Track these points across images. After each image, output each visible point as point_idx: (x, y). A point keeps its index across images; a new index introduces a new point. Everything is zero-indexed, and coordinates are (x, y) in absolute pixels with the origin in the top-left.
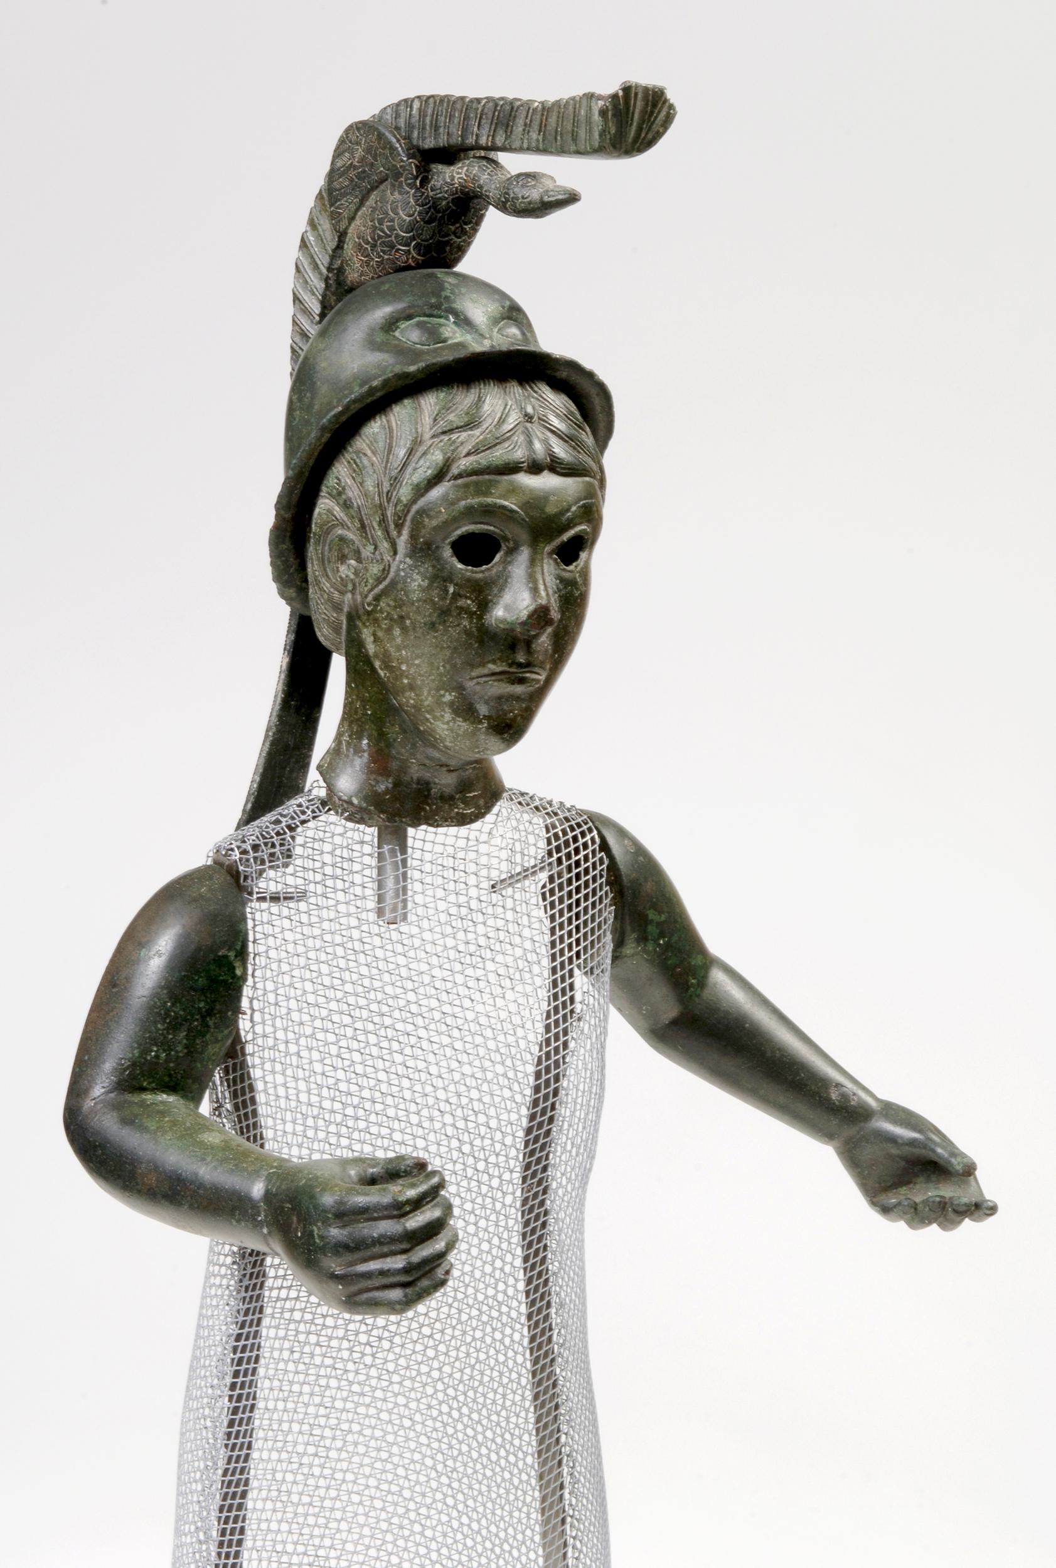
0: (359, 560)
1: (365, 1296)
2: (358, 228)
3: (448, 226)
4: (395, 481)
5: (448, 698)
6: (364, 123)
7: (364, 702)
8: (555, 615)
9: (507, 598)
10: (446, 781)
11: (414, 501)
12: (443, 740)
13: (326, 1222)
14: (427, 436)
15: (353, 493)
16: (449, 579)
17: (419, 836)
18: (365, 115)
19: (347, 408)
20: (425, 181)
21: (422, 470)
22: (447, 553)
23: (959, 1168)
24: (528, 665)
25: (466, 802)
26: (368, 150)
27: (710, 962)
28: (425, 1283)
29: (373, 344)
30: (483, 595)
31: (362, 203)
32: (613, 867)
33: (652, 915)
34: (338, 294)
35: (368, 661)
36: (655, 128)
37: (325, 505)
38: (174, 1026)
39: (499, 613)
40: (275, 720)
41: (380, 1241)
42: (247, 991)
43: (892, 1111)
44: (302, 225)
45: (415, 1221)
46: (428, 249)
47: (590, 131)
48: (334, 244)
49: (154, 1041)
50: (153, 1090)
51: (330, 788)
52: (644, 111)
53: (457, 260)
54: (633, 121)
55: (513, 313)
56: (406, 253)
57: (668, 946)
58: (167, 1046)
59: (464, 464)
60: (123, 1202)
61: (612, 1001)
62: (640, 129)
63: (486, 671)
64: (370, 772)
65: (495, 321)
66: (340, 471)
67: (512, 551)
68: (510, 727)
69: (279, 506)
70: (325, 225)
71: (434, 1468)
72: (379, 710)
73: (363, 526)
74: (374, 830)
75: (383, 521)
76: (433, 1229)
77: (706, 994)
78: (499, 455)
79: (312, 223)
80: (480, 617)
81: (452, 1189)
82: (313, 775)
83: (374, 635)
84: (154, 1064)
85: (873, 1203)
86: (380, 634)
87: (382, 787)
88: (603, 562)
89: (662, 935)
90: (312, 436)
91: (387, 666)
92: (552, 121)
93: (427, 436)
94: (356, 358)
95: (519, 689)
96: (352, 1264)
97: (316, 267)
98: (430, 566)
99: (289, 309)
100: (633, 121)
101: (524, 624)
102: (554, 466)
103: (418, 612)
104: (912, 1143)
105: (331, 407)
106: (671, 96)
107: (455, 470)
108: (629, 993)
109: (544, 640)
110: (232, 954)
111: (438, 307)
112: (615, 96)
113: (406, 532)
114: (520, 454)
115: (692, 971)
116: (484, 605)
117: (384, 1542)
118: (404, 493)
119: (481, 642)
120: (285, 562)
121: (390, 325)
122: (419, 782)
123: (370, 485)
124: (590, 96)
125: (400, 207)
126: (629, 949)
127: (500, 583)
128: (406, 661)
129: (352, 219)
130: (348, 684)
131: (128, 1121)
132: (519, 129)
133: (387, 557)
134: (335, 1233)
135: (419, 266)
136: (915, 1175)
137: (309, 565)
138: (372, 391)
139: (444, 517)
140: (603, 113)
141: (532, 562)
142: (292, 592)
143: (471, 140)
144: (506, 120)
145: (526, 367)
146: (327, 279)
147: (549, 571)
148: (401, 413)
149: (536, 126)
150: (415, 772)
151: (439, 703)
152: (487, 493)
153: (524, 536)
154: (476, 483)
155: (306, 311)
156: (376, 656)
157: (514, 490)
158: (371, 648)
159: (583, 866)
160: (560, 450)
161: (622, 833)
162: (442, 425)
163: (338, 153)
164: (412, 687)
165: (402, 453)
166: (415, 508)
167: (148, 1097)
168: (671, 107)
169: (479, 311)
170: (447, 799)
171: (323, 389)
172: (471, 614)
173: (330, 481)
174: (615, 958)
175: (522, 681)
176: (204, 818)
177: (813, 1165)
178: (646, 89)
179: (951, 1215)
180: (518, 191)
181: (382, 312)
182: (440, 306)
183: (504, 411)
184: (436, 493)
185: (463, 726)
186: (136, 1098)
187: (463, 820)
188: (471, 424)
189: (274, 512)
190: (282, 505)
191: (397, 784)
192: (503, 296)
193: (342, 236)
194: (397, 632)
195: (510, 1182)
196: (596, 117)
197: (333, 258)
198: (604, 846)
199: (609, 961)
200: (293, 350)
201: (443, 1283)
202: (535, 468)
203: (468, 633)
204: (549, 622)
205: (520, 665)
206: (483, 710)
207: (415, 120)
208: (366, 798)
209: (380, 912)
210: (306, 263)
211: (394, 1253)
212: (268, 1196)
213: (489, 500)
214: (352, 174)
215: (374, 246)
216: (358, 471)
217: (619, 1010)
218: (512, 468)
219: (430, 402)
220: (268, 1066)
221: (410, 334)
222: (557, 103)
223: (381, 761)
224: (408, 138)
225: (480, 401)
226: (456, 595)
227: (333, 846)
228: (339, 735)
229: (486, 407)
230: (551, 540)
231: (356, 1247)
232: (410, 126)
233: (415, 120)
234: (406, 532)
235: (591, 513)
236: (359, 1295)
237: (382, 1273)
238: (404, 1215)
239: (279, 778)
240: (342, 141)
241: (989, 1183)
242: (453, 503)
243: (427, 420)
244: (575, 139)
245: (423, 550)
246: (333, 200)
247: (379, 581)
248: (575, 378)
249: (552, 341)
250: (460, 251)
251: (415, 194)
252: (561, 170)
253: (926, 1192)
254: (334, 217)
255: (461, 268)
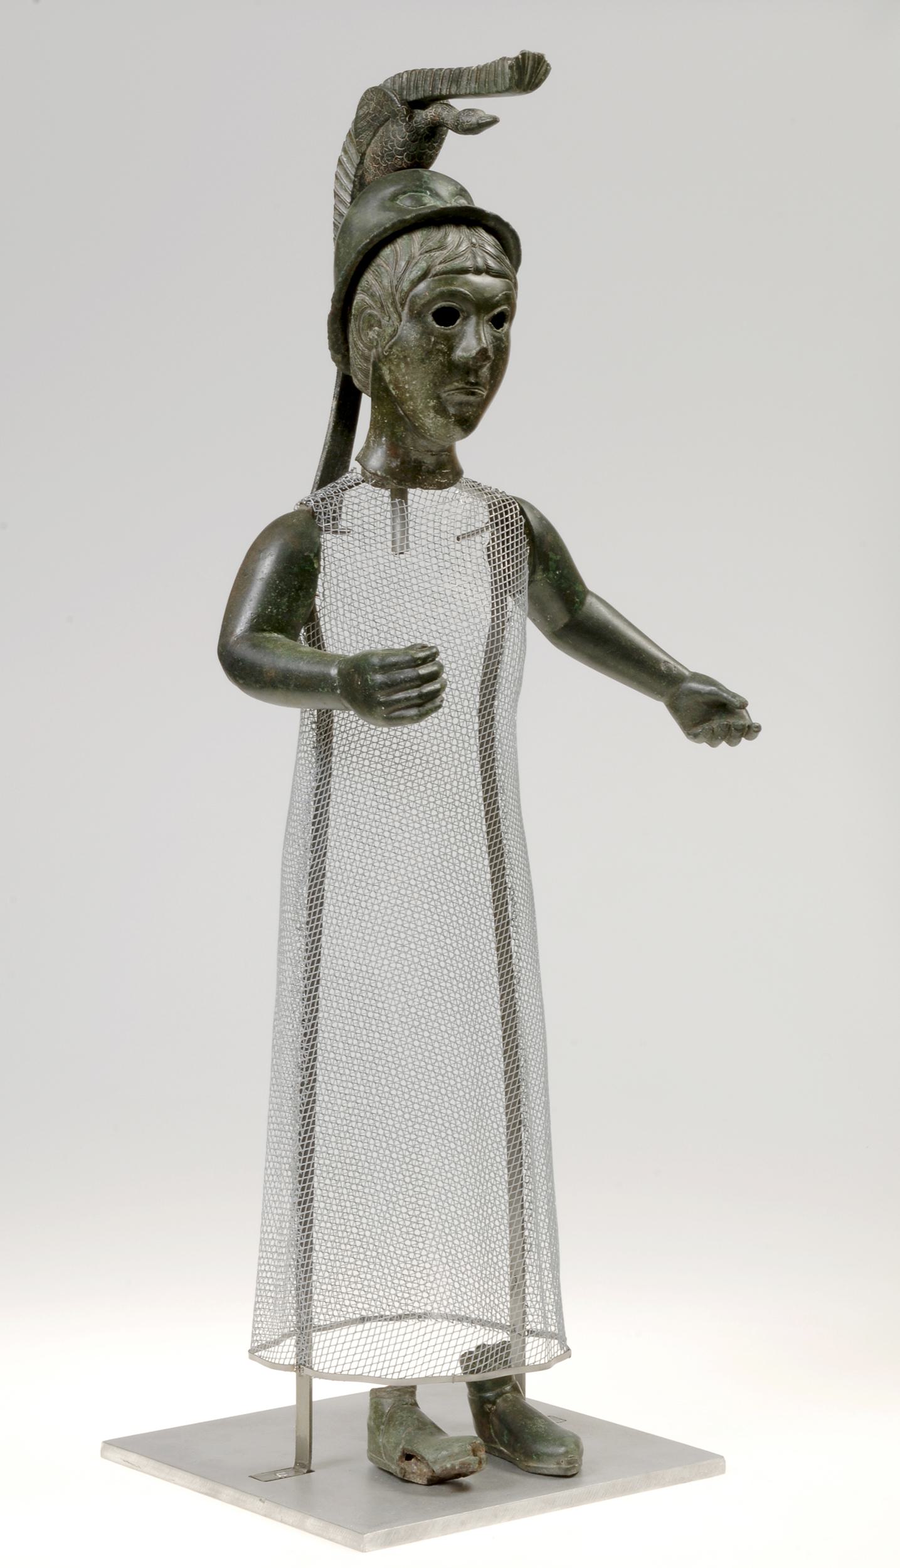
0: (380, 326)
1: (397, 713)
2: (374, 148)
3: (423, 146)
4: (400, 280)
5: (432, 403)
6: (375, 88)
7: (382, 415)
8: (490, 354)
9: (464, 344)
10: (429, 461)
11: (411, 290)
12: (429, 430)
13: (375, 672)
14: (417, 254)
15: (377, 289)
16: (431, 333)
17: (415, 495)
18: (377, 82)
19: (372, 240)
20: (411, 118)
21: (415, 273)
22: (430, 319)
23: (737, 704)
24: (477, 384)
25: (443, 476)
26: (378, 104)
27: (586, 592)
28: (429, 706)
29: (384, 208)
30: (451, 343)
31: (374, 135)
32: (528, 524)
33: (551, 555)
34: (360, 187)
35: (386, 390)
36: (539, 77)
37: (360, 297)
38: (281, 595)
39: (459, 354)
40: (329, 438)
41: (404, 681)
42: (321, 576)
43: (696, 677)
44: (339, 152)
45: (423, 671)
46: (413, 157)
47: (504, 79)
48: (358, 161)
49: (270, 603)
50: (270, 631)
51: (364, 467)
52: (533, 67)
53: (430, 164)
54: (527, 73)
55: (462, 192)
56: (402, 159)
57: (561, 576)
58: (277, 606)
59: (438, 268)
60: (256, 697)
61: (529, 615)
62: (531, 77)
63: (453, 387)
64: (388, 456)
65: (454, 195)
66: (369, 277)
67: (466, 318)
68: (467, 424)
69: (333, 301)
70: (352, 151)
71: (429, 910)
72: (394, 421)
73: (382, 306)
74: (388, 493)
75: (394, 303)
76: (433, 677)
77: (584, 609)
78: (457, 263)
79: (345, 150)
80: (449, 355)
81: (442, 655)
82: (353, 464)
83: (390, 369)
84: (270, 616)
85: (688, 734)
86: (393, 368)
87: (394, 465)
88: (518, 331)
89: (557, 568)
90: (352, 257)
91: (397, 388)
92: (483, 76)
93: (417, 254)
94: (374, 216)
95: (472, 398)
96: (389, 695)
97: (347, 175)
98: (420, 333)
99: (332, 201)
100: (527, 73)
101: (474, 358)
102: (488, 271)
103: (414, 353)
104: (710, 693)
105: (360, 241)
106: (548, 59)
107: (433, 272)
108: (538, 610)
109: (485, 371)
110: (312, 555)
111: (421, 186)
112: (517, 58)
113: (406, 308)
114: (469, 264)
115: (575, 593)
116: (451, 348)
117: (409, 902)
118: (405, 285)
119: (450, 370)
120: (336, 336)
121: (394, 197)
122: (416, 461)
123: (386, 282)
124: (504, 59)
125: (397, 133)
126: (539, 576)
127: (461, 336)
128: (408, 383)
129: (368, 145)
130: (373, 407)
131: (255, 646)
132: (464, 83)
133: (396, 323)
134: (379, 678)
135: (408, 168)
136: (713, 714)
137: (350, 336)
138: (386, 230)
139: (428, 298)
140: (511, 67)
141: (478, 324)
142: (339, 357)
143: (437, 93)
144: (458, 81)
145: (469, 217)
146: (354, 182)
147: (487, 334)
148: (401, 243)
149: (474, 78)
150: (414, 455)
151: (427, 407)
152: (451, 284)
153: (472, 309)
154: (446, 279)
155: (342, 202)
156: (390, 382)
157: (467, 283)
158: (387, 378)
159: (510, 521)
160: (492, 263)
161: (532, 508)
162: (425, 247)
163: (360, 107)
164: (411, 398)
165: (403, 264)
166: (412, 294)
167: (267, 635)
168: (548, 65)
169: (444, 190)
170: (432, 473)
171: (357, 234)
172: (444, 353)
173: (363, 283)
174: (530, 582)
175: (473, 394)
176: (292, 485)
177: (652, 713)
178: (534, 55)
179: (734, 732)
180: (465, 119)
181: (390, 191)
182: (422, 186)
183: (458, 240)
184: (422, 286)
185: (441, 420)
186: (261, 635)
187: (441, 487)
188: (442, 247)
189: (330, 304)
190: (335, 300)
191: (403, 463)
192: (456, 183)
193: (363, 155)
194: (403, 365)
195: (473, 773)
196: (507, 70)
197: (357, 169)
198: (522, 512)
199: (526, 584)
200: (335, 224)
201: (440, 707)
202: (478, 271)
203: (442, 364)
204: (488, 358)
205: (472, 384)
206: (452, 410)
207: (404, 85)
208: (385, 471)
209: (393, 549)
210: (342, 174)
211: (412, 687)
212: (339, 673)
213: (453, 288)
214: (368, 118)
215: (382, 158)
216: (378, 276)
217: (534, 620)
218: (465, 271)
219: (418, 236)
220: (333, 622)
221: (405, 202)
222: (485, 66)
223: (395, 448)
224: (401, 94)
225: (445, 236)
226: (436, 343)
227: (364, 503)
228: (368, 437)
229: (449, 239)
230: (488, 312)
231: (393, 686)
232: (401, 88)
233: (404, 85)
234: (406, 308)
235: (509, 299)
236: (393, 714)
237: (407, 699)
238: (418, 665)
239: (334, 465)
240: (362, 99)
241: (754, 714)
242: (433, 290)
243: (417, 246)
244: (495, 85)
245: (417, 316)
246: (357, 135)
247: (392, 337)
248: (498, 227)
249: (483, 201)
250: (432, 159)
251: (407, 124)
252: (486, 106)
253: (717, 723)
254: (359, 144)
255: (432, 169)
